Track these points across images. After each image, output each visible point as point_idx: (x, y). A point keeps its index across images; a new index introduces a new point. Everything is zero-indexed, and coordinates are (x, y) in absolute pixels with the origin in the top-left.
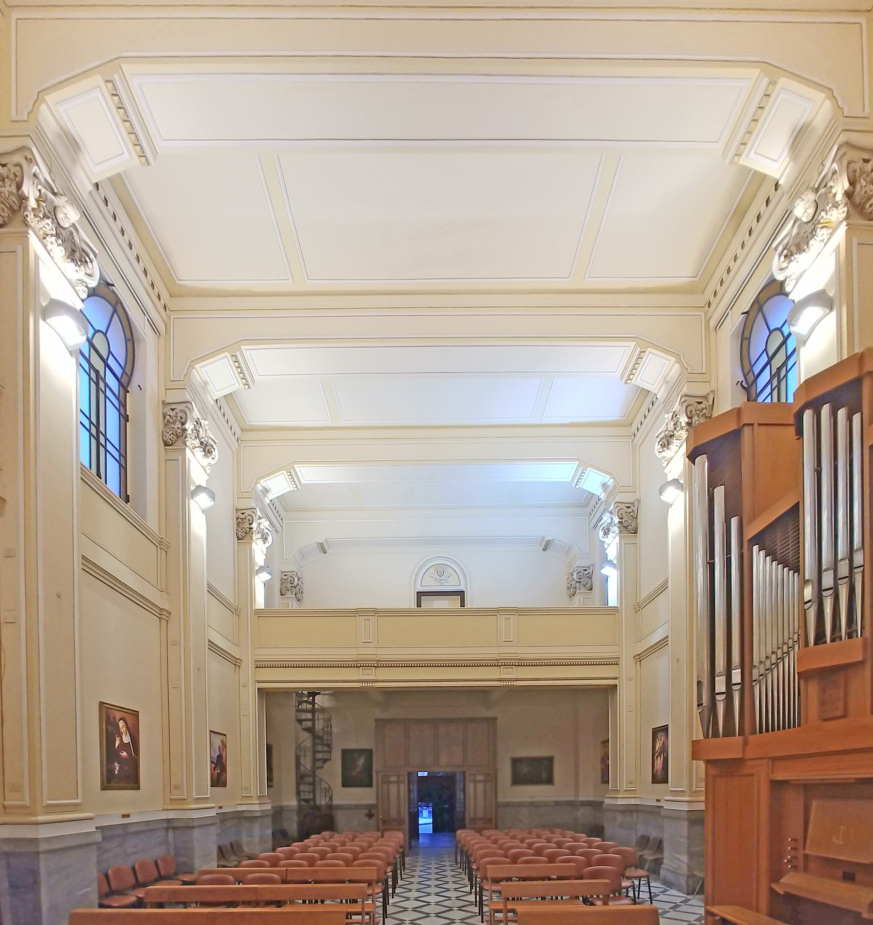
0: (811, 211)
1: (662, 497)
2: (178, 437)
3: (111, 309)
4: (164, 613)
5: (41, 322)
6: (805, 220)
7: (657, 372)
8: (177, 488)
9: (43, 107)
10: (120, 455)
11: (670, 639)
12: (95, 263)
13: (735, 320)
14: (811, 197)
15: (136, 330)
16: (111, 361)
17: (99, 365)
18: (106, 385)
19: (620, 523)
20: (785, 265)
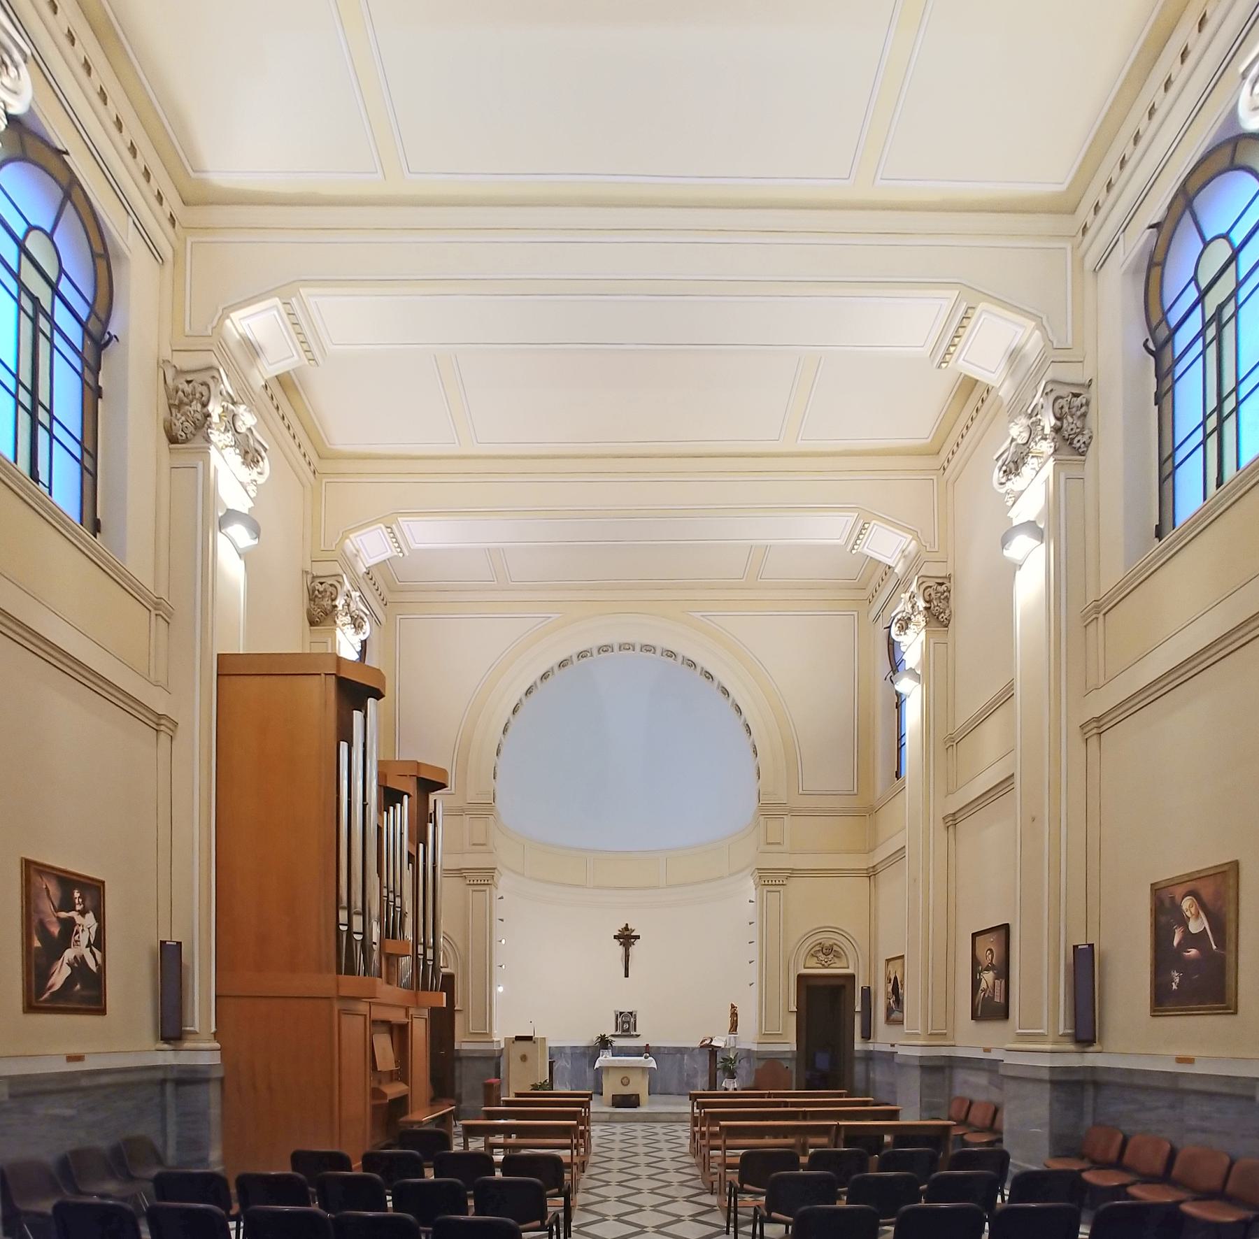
0: (1026, 435)
1: (1006, 553)
2: (196, 428)
3: (59, 194)
4: (163, 722)
5: (219, 534)
6: (1020, 441)
7: (994, 345)
8: (195, 516)
9: (228, 322)
10: (83, 449)
11: (1017, 777)
12: (266, 460)
13: (1138, 239)
14: (1024, 421)
15: (109, 232)
16: (64, 287)
17: (42, 292)
18: (54, 326)
19: (926, 608)
20: (1003, 480)
